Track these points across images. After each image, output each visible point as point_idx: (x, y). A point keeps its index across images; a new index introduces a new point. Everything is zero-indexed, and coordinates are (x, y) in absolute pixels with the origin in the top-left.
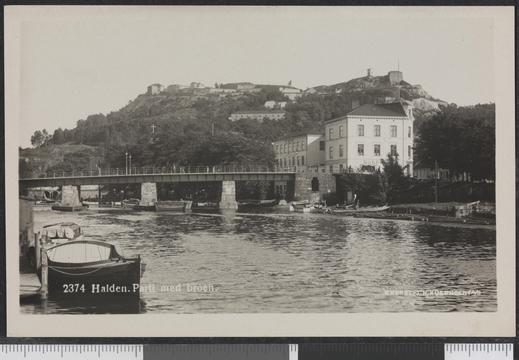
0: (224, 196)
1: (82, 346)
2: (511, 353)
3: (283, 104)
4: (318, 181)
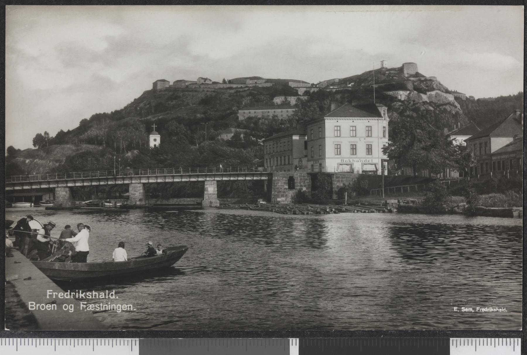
0: (207, 196)
1: (76, 339)
2: (519, 348)
3: (293, 100)
4: (294, 180)
